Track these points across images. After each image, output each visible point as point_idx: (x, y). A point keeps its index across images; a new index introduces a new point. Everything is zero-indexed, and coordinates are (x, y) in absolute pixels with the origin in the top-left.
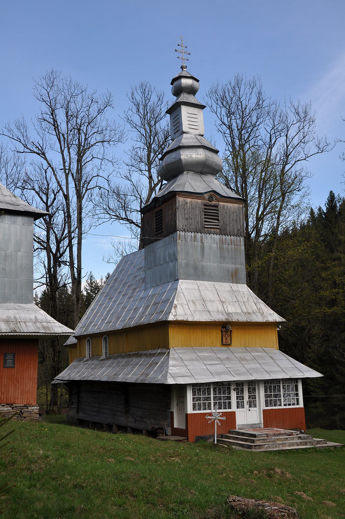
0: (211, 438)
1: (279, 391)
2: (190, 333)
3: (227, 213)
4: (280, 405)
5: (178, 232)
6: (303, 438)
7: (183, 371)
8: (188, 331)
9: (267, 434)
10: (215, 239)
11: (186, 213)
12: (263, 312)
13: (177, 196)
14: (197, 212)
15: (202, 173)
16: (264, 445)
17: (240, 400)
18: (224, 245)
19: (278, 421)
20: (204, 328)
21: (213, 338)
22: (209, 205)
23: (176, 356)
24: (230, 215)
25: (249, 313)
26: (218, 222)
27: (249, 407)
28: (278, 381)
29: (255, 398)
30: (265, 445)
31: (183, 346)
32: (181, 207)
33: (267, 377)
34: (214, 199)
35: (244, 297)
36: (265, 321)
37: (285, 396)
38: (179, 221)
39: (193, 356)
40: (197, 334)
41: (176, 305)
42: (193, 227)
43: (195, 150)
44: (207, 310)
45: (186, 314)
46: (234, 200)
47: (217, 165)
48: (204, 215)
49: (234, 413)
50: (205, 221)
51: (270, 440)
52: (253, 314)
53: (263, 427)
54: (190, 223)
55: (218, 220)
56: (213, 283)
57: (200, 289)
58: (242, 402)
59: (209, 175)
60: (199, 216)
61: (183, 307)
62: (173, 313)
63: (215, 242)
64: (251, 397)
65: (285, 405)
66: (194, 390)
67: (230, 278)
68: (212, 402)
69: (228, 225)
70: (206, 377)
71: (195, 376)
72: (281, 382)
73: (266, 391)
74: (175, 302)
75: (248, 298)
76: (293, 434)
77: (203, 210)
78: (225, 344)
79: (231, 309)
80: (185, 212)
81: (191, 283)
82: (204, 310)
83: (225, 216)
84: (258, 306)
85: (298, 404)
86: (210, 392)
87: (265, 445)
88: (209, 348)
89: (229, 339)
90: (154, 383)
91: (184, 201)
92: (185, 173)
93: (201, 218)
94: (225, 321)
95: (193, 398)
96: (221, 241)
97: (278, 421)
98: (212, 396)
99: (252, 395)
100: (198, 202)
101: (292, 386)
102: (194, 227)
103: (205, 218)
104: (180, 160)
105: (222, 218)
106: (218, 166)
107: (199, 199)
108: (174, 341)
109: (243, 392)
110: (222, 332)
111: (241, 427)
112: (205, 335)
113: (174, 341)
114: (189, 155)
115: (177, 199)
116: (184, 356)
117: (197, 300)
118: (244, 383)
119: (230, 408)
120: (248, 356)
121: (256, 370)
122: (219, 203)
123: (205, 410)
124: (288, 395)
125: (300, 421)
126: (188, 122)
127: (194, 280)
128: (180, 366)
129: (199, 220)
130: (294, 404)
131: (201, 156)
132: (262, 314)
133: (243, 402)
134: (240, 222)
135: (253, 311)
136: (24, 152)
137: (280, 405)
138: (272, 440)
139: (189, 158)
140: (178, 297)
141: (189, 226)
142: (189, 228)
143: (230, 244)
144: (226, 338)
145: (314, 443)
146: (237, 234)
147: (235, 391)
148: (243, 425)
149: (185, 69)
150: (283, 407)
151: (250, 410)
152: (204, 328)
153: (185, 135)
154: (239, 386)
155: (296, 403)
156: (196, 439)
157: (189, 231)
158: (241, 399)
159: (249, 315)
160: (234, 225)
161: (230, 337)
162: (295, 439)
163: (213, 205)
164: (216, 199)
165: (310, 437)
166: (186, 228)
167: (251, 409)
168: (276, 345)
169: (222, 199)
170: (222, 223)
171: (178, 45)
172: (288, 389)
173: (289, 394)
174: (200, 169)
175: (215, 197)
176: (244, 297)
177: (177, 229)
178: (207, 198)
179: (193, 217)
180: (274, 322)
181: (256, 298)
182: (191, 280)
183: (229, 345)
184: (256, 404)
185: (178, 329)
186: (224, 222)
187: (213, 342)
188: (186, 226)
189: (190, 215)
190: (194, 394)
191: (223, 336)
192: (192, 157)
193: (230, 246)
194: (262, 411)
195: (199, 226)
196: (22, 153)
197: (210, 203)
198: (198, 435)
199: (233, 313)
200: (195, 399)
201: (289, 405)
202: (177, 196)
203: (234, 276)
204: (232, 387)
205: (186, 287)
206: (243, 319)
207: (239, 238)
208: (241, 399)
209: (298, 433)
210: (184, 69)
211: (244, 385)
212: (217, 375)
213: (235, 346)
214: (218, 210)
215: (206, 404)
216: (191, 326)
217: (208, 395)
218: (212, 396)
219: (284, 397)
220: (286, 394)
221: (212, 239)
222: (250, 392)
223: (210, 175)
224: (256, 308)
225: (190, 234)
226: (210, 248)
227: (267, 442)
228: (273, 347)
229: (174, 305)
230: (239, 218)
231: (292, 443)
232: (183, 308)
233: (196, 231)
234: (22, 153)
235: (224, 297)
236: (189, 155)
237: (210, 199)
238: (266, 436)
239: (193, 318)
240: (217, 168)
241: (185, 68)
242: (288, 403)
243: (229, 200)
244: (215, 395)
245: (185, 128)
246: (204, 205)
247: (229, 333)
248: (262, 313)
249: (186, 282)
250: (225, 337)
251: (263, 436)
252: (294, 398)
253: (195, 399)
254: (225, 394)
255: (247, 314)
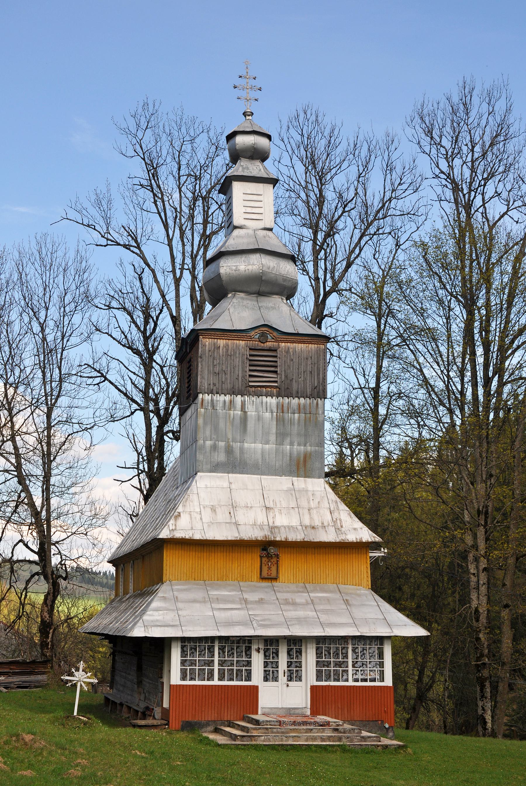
0: (209, 725)
1: (213, 656)
2: (202, 560)
3: (294, 360)
4: (347, 680)
5: (200, 396)
6: (342, 731)
7: (169, 617)
8: (199, 556)
9: (280, 721)
10: (268, 404)
11: (215, 363)
12: (342, 526)
13: (201, 337)
14: (238, 361)
15: (260, 294)
16: (259, 736)
17: (272, 668)
18: (286, 415)
19: (340, 706)
20: (228, 551)
21: (245, 567)
22: (260, 348)
23: (169, 595)
24: (299, 364)
25: (313, 528)
26: (275, 376)
27: (288, 681)
28: (344, 639)
29: (301, 667)
30: (262, 736)
31: (189, 579)
32: (207, 355)
33: (318, 632)
34: (269, 337)
35: (311, 501)
36: (338, 541)
37: (356, 665)
38: (203, 378)
39: (199, 594)
40: (216, 560)
41: (179, 513)
42: (228, 386)
43: (246, 257)
44: (234, 521)
45: (192, 528)
46: (307, 338)
47: (285, 279)
48: (250, 365)
49: (255, 689)
50: (250, 376)
51: (279, 730)
52: (320, 529)
53: (309, 713)
54: (223, 380)
55: (276, 372)
56: (259, 476)
57: (233, 486)
58: (275, 672)
59: (274, 296)
60: (240, 367)
61: (191, 517)
62: (171, 526)
63: (268, 409)
64: (293, 665)
65: (356, 680)
66: (318, 652)
67: (294, 468)
68: (216, 668)
69: (294, 381)
70: (203, 628)
71: (184, 626)
72: (350, 642)
73: (319, 655)
74: (180, 509)
75: (319, 502)
76: (331, 724)
77: (248, 357)
78: (266, 576)
79: (281, 520)
80: (213, 362)
81: (218, 477)
82: (228, 521)
83: (289, 366)
84: (336, 515)
85: (382, 680)
86: (347, 653)
87: (262, 736)
88: (236, 582)
89: (274, 569)
90: (116, 636)
91: (214, 344)
92: (230, 295)
93: (244, 371)
94: (262, 540)
95: (317, 662)
96: (280, 407)
97: (340, 706)
98: (216, 659)
99: (296, 662)
100: (239, 346)
101: (373, 649)
102: (229, 386)
103: (250, 370)
104: (219, 275)
105: (283, 369)
106: (289, 281)
107: (242, 340)
108: (174, 570)
109: (277, 656)
110: (261, 557)
111: (267, 711)
112: (231, 563)
113: (174, 570)
114: (235, 266)
115: (200, 343)
116: (181, 596)
117: (220, 506)
118: (280, 641)
119: (383, 681)
120: (301, 598)
121: (300, 621)
122: (279, 345)
123: (230, 680)
124: (363, 664)
125: (383, 709)
126: (244, 209)
127: (225, 473)
128: (166, 610)
129: (240, 375)
130: (373, 680)
131: (254, 267)
132: (338, 530)
133: (277, 671)
134: (318, 374)
135: (323, 524)
136: (107, 245)
137: (347, 680)
138: (283, 730)
139: (233, 272)
140: (186, 501)
141: (220, 384)
142: (220, 388)
143: (296, 411)
144: (269, 568)
145: (355, 739)
146: (311, 395)
147: (259, 652)
148: (271, 708)
149: (250, 118)
150: (350, 683)
151: (288, 686)
152: (228, 551)
153: (236, 232)
154: (295, 644)
155: (378, 677)
156: (182, 726)
157: (220, 392)
158: (274, 666)
159: (313, 531)
160: (305, 380)
161: (275, 565)
162: (326, 732)
163: (268, 348)
164: (273, 339)
165: (356, 731)
166: (215, 388)
167: (290, 683)
168: (367, 580)
169: (281, 337)
170: (283, 377)
171: (240, 77)
172: (193, 653)
173: (365, 663)
174: (255, 288)
175: (271, 335)
176: (311, 501)
177: (198, 391)
178: (257, 337)
179: (229, 369)
180: (357, 543)
181: (336, 502)
182: (219, 473)
183: (275, 579)
184: (301, 677)
185: (180, 552)
186: (286, 377)
187: (244, 574)
188: (214, 385)
189: (224, 367)
190: (184, 653)
191: (263, 565)
192: (239, 270)
193: (296, 415)
194: (309, 687)
195: (239, 384)
196: (105, 246)
197: (262, 345)
198: (187, 720)
199: (283, 529)
200: (188, 663)
201: (366, 680)
202: (201, 337)
203: (301, 465)
204: (254, 647)
205: (206, 485)
206: (293, 537)
207: (315, 402)
208: (274, 666)
209: (341, 723)
210: (248, 118)
211: (280, 644)
212: (224, 626)
213: (286, 581)
214: (276, 357)
215: (322, 672)
216: (191, 548)
217: (343, 659)
218: (216, 659)
219: (353, 666)
220: (359, 663)
221: (264, 404)
222: (292, 657)
223: (277, 296)
224: (330, 518)
225: (269, 399)
226: (259, 418)
227: (273, 732)
228: (360, 585)
229: (176, 514)
230: (316, 367)
231: (313, 736)
232: (191, 519)
233: (233, 392)
234: (105, 246)
235: (273, 501)
236: (235, 266)
237: (263, 338)
238: (279, 724)
239: (203, 535)
240: (289, 284)
241: (249, 115)
242: (369, 677)
243: (297, 338)
244: (185, 657)
245: (238, 219)
246: (250, 349)
247: (275, 560)
248: (340, 527)
249: (210, 476)
250: (267, 566)
251: (273, 723)
252: (375, 670)
253: (203, 663)
254: (338, 658)
255: (309, 529)
